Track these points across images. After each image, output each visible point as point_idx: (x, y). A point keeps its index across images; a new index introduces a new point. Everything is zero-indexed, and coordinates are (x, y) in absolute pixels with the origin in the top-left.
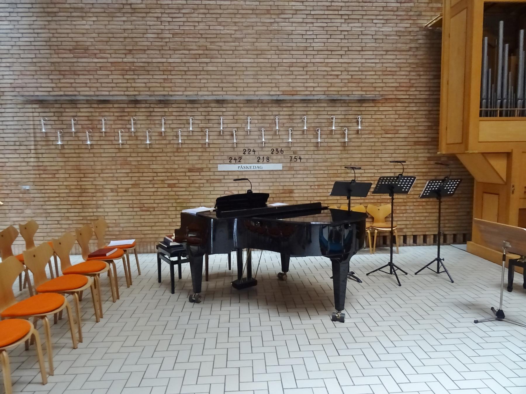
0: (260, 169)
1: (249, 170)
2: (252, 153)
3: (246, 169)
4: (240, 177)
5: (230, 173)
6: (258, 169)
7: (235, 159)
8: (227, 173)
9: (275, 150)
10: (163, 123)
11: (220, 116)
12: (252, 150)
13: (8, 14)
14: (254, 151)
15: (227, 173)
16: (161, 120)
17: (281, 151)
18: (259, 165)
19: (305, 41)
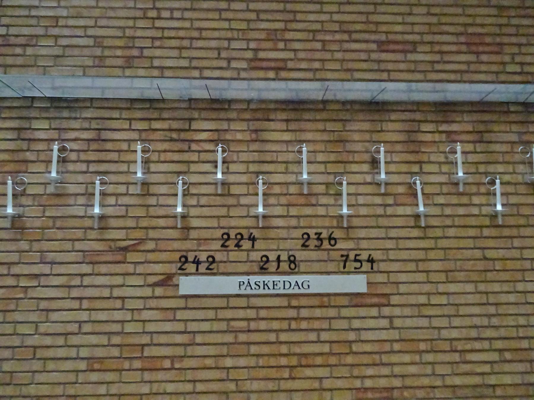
0: (302, 291)
1: (272, 292)
2: (246, 244)
3: (261, 291)
4: (419, 330)
5: (192, 303)
6: (297, 291)
7: (197, 262)
8: (223, 303)
9: (313, 236)
10: (260, 193)
11: (412, 174)
12: (246, 236)
13: (497, 30)
14: (253, 239)
15: (223, 303)
16: (175, 184)
17: (330, 238)
18: (269, 279)
19: (216, 56)
